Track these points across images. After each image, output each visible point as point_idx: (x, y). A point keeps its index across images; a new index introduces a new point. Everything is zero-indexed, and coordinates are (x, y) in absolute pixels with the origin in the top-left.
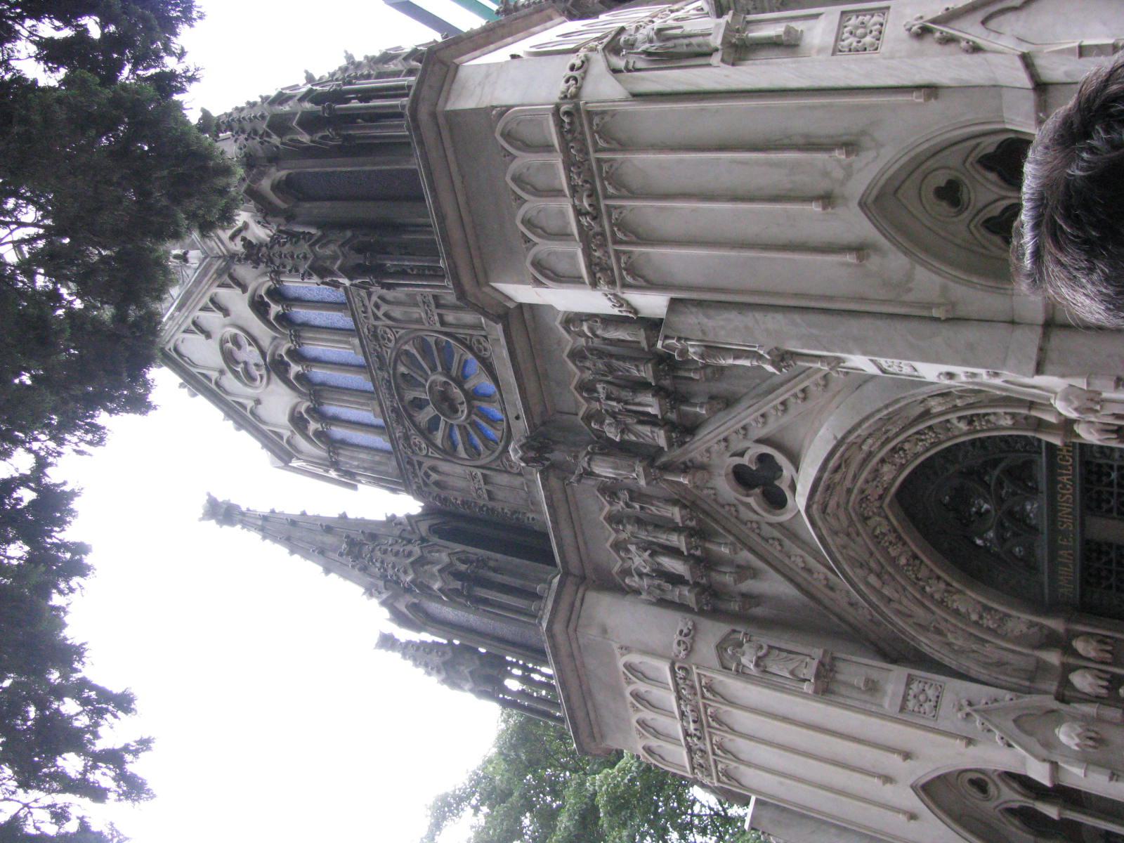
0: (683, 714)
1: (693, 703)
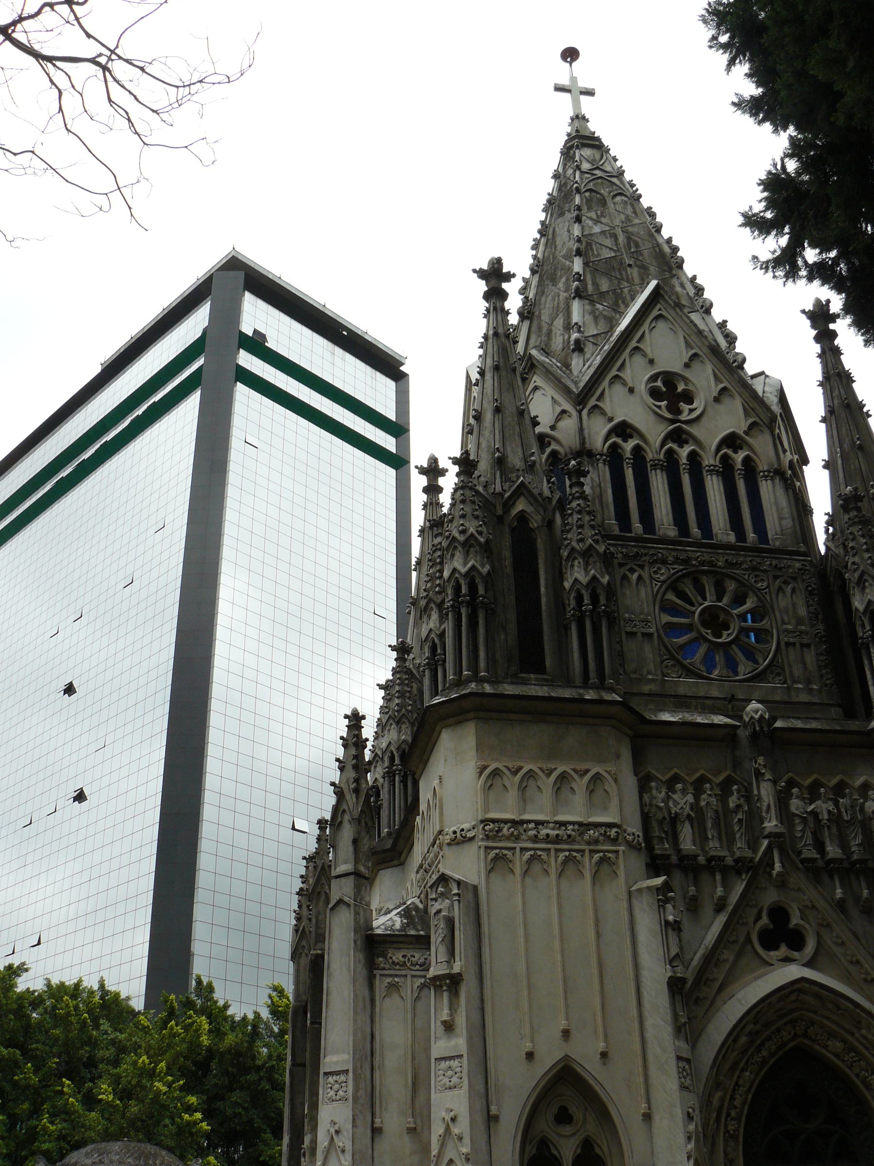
0: (563, 824)
1: (578, 838)
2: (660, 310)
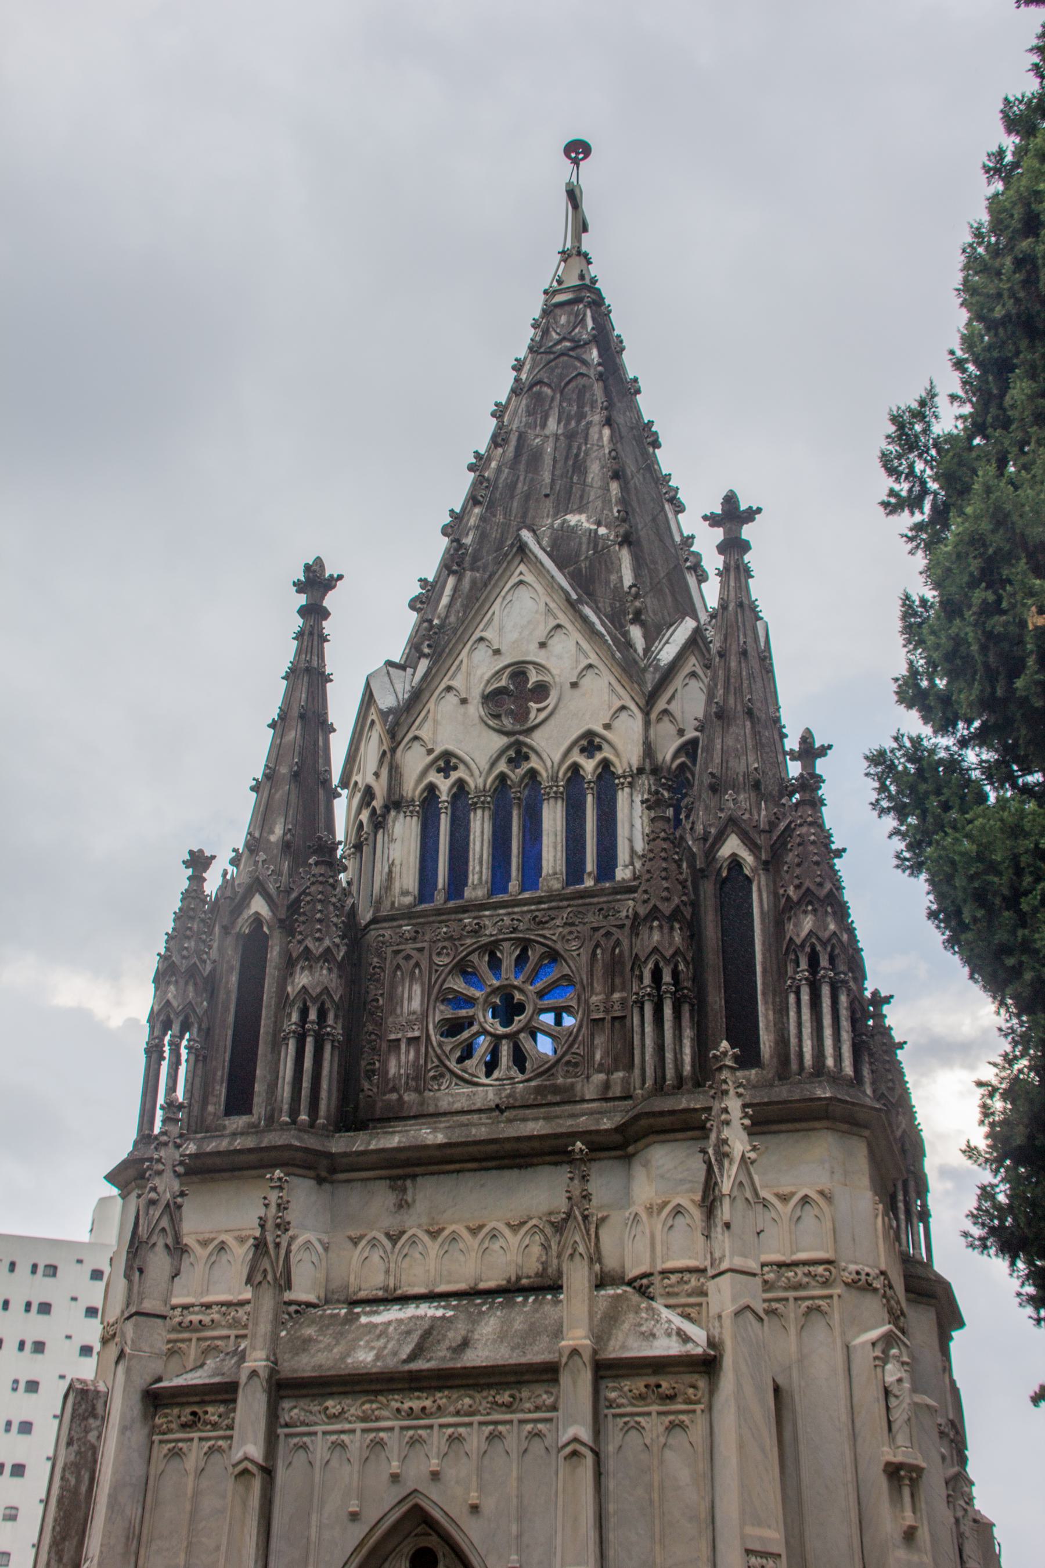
0: (208, 1306)
2: (521, 573)
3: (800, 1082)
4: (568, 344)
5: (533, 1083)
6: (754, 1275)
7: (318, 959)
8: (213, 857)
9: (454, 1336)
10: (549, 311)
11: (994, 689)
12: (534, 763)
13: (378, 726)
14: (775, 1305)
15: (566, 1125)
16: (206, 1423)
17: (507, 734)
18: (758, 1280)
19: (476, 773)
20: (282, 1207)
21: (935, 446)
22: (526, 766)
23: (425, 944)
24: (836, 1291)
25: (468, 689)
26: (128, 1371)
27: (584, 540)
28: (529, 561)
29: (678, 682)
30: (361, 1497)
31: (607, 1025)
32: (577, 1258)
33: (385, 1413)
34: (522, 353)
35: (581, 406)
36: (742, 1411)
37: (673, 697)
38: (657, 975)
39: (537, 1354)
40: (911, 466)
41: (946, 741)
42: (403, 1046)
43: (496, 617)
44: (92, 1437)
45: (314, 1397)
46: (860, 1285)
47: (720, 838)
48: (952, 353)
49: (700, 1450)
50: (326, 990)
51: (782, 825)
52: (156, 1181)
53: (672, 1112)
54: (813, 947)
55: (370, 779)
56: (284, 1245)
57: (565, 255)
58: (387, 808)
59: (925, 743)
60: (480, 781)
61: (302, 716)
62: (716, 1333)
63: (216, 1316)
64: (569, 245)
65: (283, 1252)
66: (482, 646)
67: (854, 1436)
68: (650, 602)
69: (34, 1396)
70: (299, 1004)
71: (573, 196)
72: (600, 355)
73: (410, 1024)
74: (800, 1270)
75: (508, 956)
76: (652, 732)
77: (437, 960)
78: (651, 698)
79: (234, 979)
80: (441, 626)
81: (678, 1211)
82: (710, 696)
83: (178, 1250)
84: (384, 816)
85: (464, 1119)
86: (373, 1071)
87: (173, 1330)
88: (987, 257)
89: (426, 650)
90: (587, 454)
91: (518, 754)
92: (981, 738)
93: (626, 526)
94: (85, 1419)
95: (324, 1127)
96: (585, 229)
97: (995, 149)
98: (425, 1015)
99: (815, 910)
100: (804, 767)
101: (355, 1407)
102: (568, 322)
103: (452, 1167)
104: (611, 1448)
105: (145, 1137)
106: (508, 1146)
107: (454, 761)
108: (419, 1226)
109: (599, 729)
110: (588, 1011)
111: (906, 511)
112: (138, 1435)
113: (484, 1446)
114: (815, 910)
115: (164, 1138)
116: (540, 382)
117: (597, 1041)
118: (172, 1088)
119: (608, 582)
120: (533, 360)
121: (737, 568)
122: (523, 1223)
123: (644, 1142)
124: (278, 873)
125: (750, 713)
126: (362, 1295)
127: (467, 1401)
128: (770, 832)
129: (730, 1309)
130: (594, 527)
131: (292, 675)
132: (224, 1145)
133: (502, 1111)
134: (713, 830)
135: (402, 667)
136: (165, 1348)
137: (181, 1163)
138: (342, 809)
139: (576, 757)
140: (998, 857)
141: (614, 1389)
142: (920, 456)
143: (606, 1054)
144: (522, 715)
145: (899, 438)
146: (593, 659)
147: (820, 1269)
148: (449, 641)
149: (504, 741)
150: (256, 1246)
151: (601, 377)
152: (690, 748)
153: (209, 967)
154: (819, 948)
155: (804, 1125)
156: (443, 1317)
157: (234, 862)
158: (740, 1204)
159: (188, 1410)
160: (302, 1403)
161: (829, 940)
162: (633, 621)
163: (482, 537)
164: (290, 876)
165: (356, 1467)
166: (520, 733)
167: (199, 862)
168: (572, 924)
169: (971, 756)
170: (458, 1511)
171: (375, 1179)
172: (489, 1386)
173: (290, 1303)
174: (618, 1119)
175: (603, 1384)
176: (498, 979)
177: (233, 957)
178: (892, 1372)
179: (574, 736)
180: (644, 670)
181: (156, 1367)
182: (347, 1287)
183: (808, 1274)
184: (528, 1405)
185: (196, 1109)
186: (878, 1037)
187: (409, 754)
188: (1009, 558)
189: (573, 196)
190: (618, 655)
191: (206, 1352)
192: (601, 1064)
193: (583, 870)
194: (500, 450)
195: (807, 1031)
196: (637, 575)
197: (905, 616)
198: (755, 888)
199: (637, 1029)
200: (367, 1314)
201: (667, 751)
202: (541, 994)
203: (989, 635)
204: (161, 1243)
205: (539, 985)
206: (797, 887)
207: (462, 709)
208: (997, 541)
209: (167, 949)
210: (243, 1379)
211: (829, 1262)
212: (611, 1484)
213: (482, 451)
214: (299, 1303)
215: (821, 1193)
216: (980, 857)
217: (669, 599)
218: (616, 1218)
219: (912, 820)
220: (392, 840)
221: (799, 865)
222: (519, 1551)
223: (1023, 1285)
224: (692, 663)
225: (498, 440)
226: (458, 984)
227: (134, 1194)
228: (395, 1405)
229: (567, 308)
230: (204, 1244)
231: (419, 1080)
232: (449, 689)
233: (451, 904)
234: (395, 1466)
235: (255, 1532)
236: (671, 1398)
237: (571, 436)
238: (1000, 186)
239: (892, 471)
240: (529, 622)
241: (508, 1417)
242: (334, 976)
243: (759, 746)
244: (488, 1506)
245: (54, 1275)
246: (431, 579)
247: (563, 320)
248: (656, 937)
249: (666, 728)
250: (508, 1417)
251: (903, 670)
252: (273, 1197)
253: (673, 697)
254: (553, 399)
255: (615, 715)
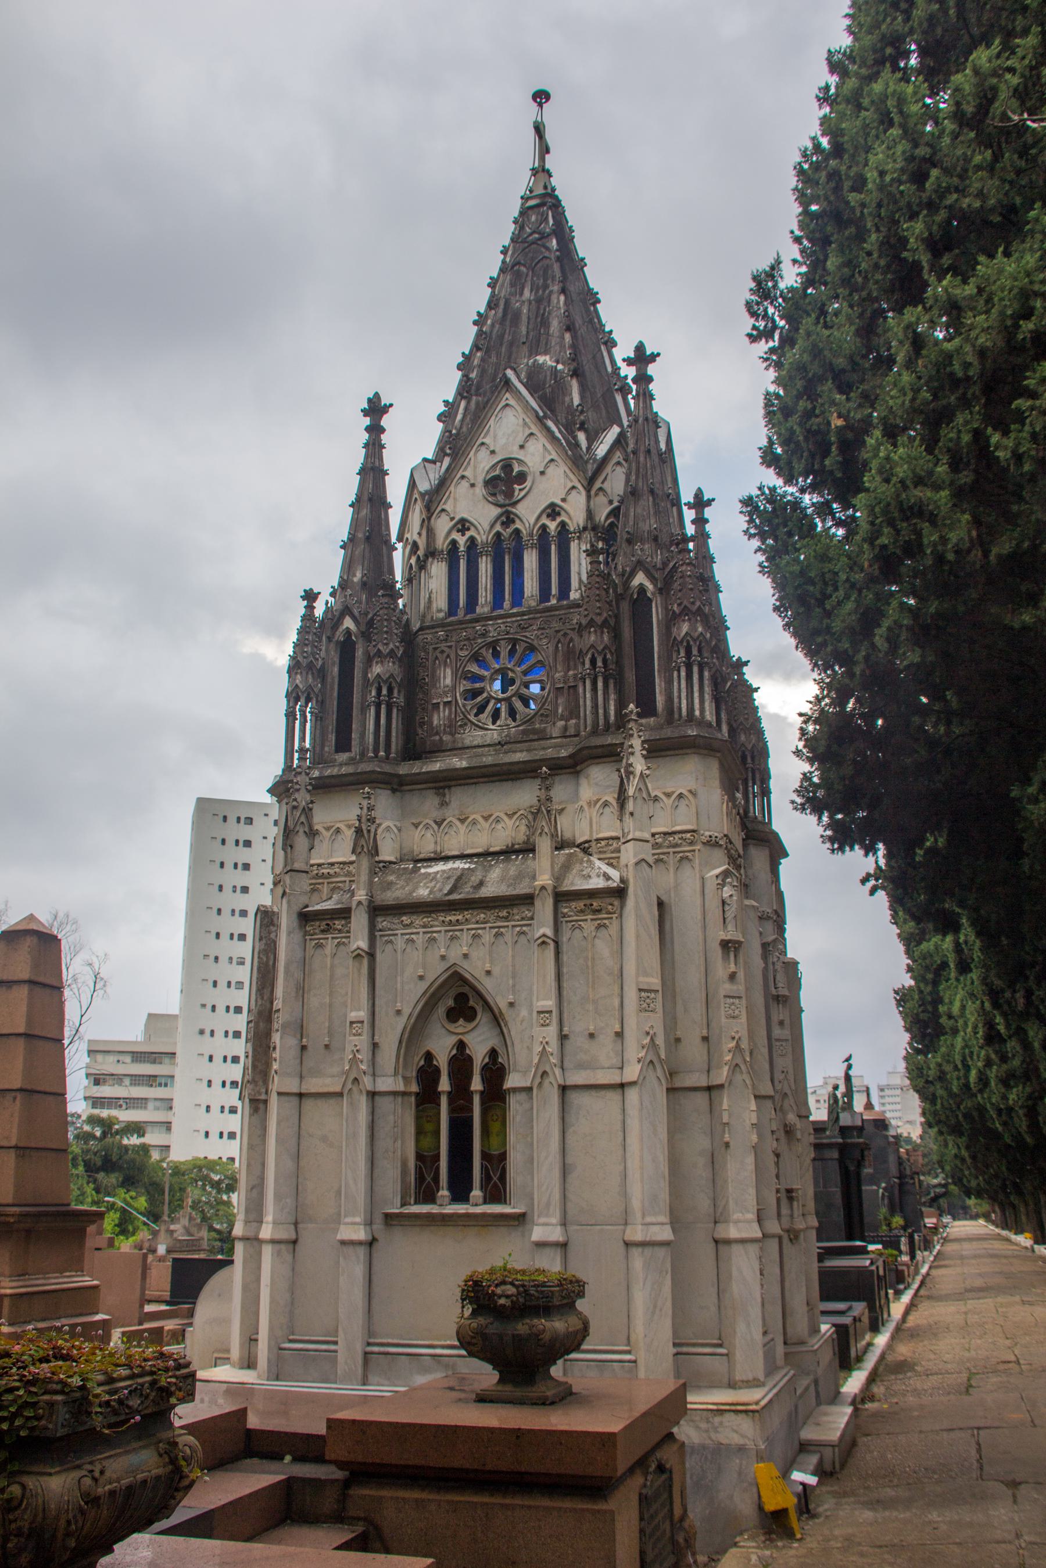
0: (332, 864)
3: (679, 725)
4: (537, 236)
5: (521, 728)
6: (648, 841)
7: (386, 657)
8: (319, 593)
9: (475, 879)
10: (524, 212)
11: (813, 465)
12: (518, 525)
13: (419, 502)
14: (662, 857)
15: (539, 755)
16: (335, 929)
17: (501, 506)
18: (650, 845)
19: (482, 532)
20: (370, 809)
21: (781, 296)
22: (513, 527)
23: (453, 644)
24: (697, 847)
25: (475, 477)
26: (289, 902)
27: (548, 373)
28: (512, 391)
29: (608, 469)
30: (424, 968)
31: (565, 691)
32: (544, 835)
33: (436, 923)
34: (507, 242)
35: (545, 280)
36: (638, 916)
37: (606, 478)
38: (593, 661)
39: (522, 889)
40: (766, 310)
41: (791, 489)
42: (441, 707)
43: (492, 429)
44: (273, 936)
45: (395, 915)
46: (712, 843)
47: (632, 574)
48: (792, 232)
49: (615, 938)
50: (392, 676)
51: (671, 564)
52: (297, 795)
53: (603, 746)
54: (688, 642)
55: (416, 537)
56: (373, 830)
57: (535, 172)
58: (426, 556)
59: (778, 491)
60: (484, 537)
61: (370, 500)
62: (625, 875)
63: (337, 870)
64: (536, 165)
65: (372, 835)
66: (483, 448)
67: (705, 927)
68: (591, 415)
69: (246, 895)
70: (376, 685)
71: (539, 130)
72: (558, 243)
73: (445, 693)
74: (677, 837)
75: (504, 649)
76: (592, 503)
77: (461, 653)
78: (591, 481)
79: (336, 669)
80: (458, 434)
81: (606, 804)
82: (628, 480)
83: (312, 834)
84: (425, 561)
85: (480, 750)
86: (424, 723)
87: (314, 878)
88: (810, 172)
89: (448, 451)
90: (549, 313)
91: (508, 519)
92: (814, 488)
93: (575, 364)
94: (268, 926)
95: (395, 759)
96: (548, 151)
97: (823, 85)
98: (454, 687)
99: (689, 619)
100: (697, 513)
101: (419, 920)
102: (537, 220)
103: (472, 781)
104: (565, 939)
105: (288, 768)
106: (505, 768)
107: (467, 524)
108: (454, 816)
109: (559, 502)
110: (553, 683)
111: (764, 340)
112: (298, 936)
113: (493, 939)
114: (689, 619)
115: (299, 770)
116: (519, 263)
117: (559, 701)
118: (303, 739)
119: (563, 402)
120: (514, 247)
121: (644, 394)
122: (515, 813)
123: (586, 764)
124: (359, 602)
125: (652, 492)
126: (422, 856)
127: (482, 916)
128: (664, 569)
129: (633, 861)
130: (554, 364)
131: (363, 472)
132: (335, 771)
133: (503, 746)
134: (628, 569)
135: (433, 462)
136: (309, 889)
137: (310, 784)
138: (398, 558)
139: (545, 520)
140: (812, 574)
141: (566, 907)
142: (771, 303)
143: (565, 709)
144: (509, 493)
145: (758, 290)
146: (554, 456)
147: (688, 835)
148: (462, 445)
149: (499, 510)
150: (357, 832)
151: (558, 259)
152: (615, 513)
153: (320, 663)
154: (692, 643)
155: (681, 752)
156: (469, 869)
157: (333, 595)
158: (639, 801)
159: (324, 923)
160: (389, 918)
161: (698, 637)
162: (580, 429)
163: (483, 372)
164: (367, 603)
165: (421, 952)
166: (509, 505)
167: (310, 597)
168: (543, 629)
169: (807, 499)
170: (479, 974)
171: (426, 789)
172: (495, 907)
173: (380, 862)
174: (571, 750)
175: (560, 905)
176: (498, 663)
177: (335, 657)
178: (727, 891)
179: (543, 507)
180: (587, 462)
181: (304, 900)
182: (413, 852)
183: (682, 838)
184: (517, 917)
185: (318, 749)
186: (740, 688)
187: (439, 521)
188: (822, 379)
189: (539, 130)
190: (570, 453)
191: (333, 890)
192: (562, 715)
193: (550, 594)
194: (493, 312)
195: (684, 695)
196: (582, 397)
197: (766, 406)
198: (654, 605)
199: (581, 695)
200: (425, 867)
201: (602, 515)
202: (525, 673)
203: (809, 431)
204: (301, 830)
205: (524, 667)
206: (679, 605)
207: (471, 491)
208: (815, 369)
209: (294, 652)
210: (354, 907)
211: (694, 831)
212: (565, 958)
213: (482, 311)
214: (385, 862)
215: (690, 791)
216: (802, 573)
217: (604, 412)
218: (571, 808)
219: (770, 542)
220: (431, 577)
221: (680, 591)
222: (514, 993)
223: (825, 831)
224: (618, 456)
225: (492, 304)
226: (474, 668)
227: (285, 801)
228: (441, 919)
229: (536, 210)
230: (328, 829)
231: (452, 727)
232: (463, 477)
233: (468, 617)
234: (443, 951)
235: (366, 986)
236: (599, 911)
237: (539, 301)
238: (828, 110)
239: (753, 314)
240: (513, 432)
241: (506, 924)
242: (396, 666)
243: (657, 513)
244: (496, 971)
245: (251, 823)
246: (451, 400)
247: (533, 218)
248: (593, 638)
249: (601, 499)
250: (506, 924)
251: (764, 442)
252: (365, 803)
253: (606, 478)
254: (527, 275)
255: (568, 493)
